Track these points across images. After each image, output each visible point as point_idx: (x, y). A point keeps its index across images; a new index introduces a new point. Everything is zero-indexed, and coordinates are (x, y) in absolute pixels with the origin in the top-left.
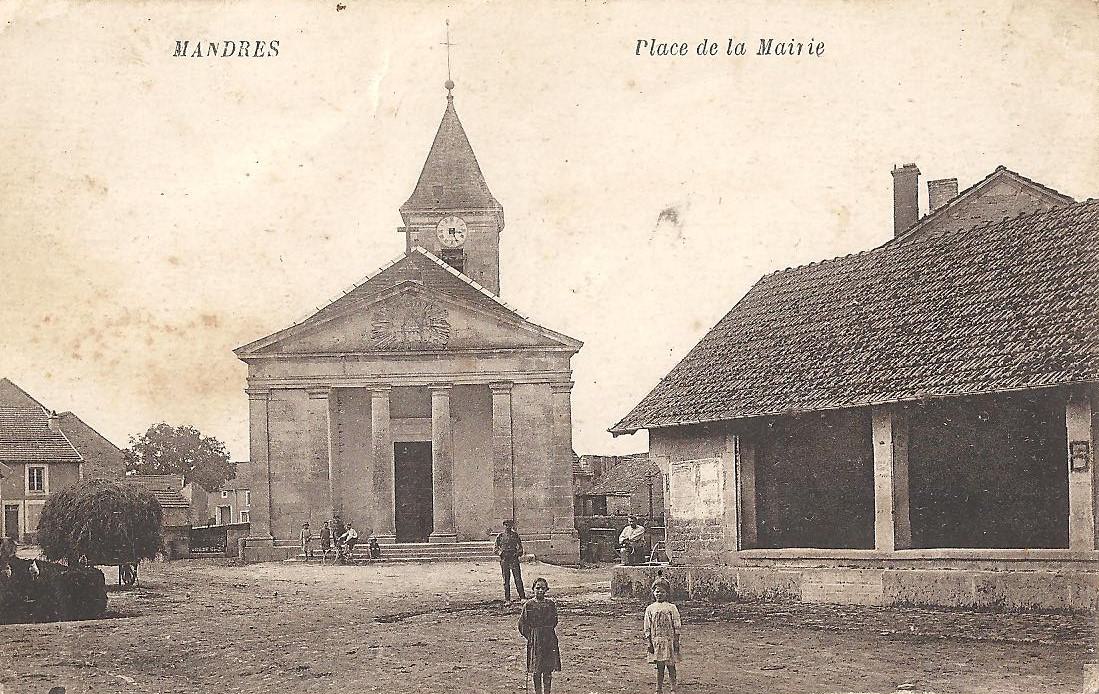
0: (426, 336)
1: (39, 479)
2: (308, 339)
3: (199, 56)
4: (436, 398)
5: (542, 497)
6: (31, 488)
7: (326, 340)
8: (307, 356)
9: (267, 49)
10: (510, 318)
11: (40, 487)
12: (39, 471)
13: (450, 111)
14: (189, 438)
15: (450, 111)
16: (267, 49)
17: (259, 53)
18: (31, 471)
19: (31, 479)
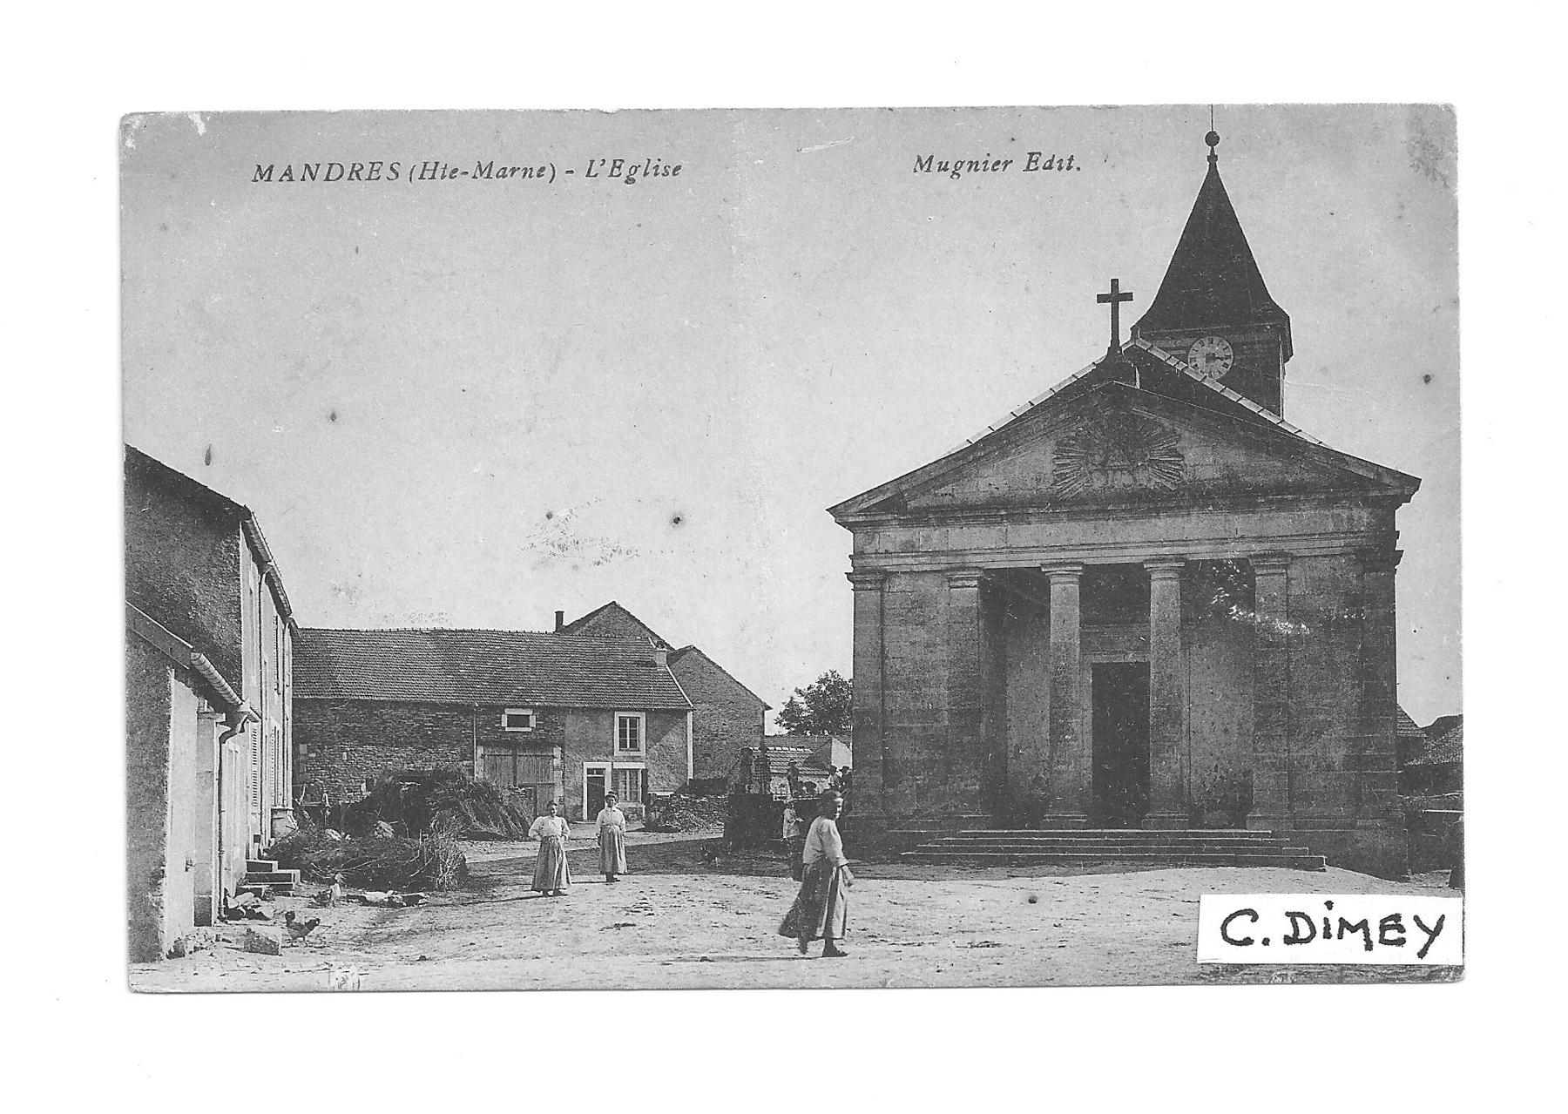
0: (1142, 477)
1: (634, 734)
2: (948, 489)
3: (291, 180)
4: (1159, 582)
5: (1338, 755)
6: (623, 745)
7: (952, 492)
8: (945, 515)
9: (385, 172)
10: (1292, 446)
11: (634, 745)
12: (634, 722)
13: (1213, 176)
14: (1352, 932)
15: (1213, 176)
16: (385, 172)
17: (1033, 166)
18: (622, 721)
19: (622, 733)
